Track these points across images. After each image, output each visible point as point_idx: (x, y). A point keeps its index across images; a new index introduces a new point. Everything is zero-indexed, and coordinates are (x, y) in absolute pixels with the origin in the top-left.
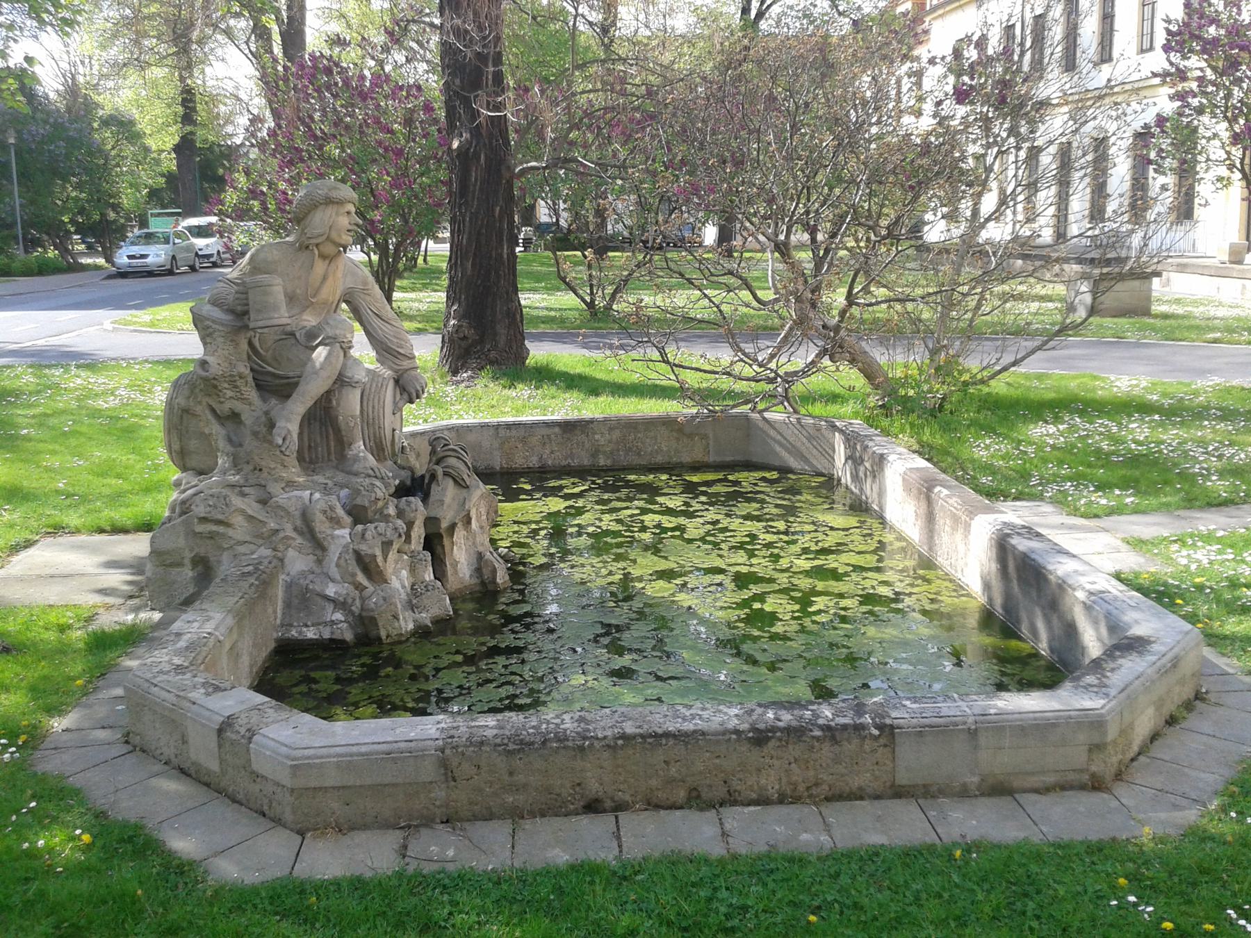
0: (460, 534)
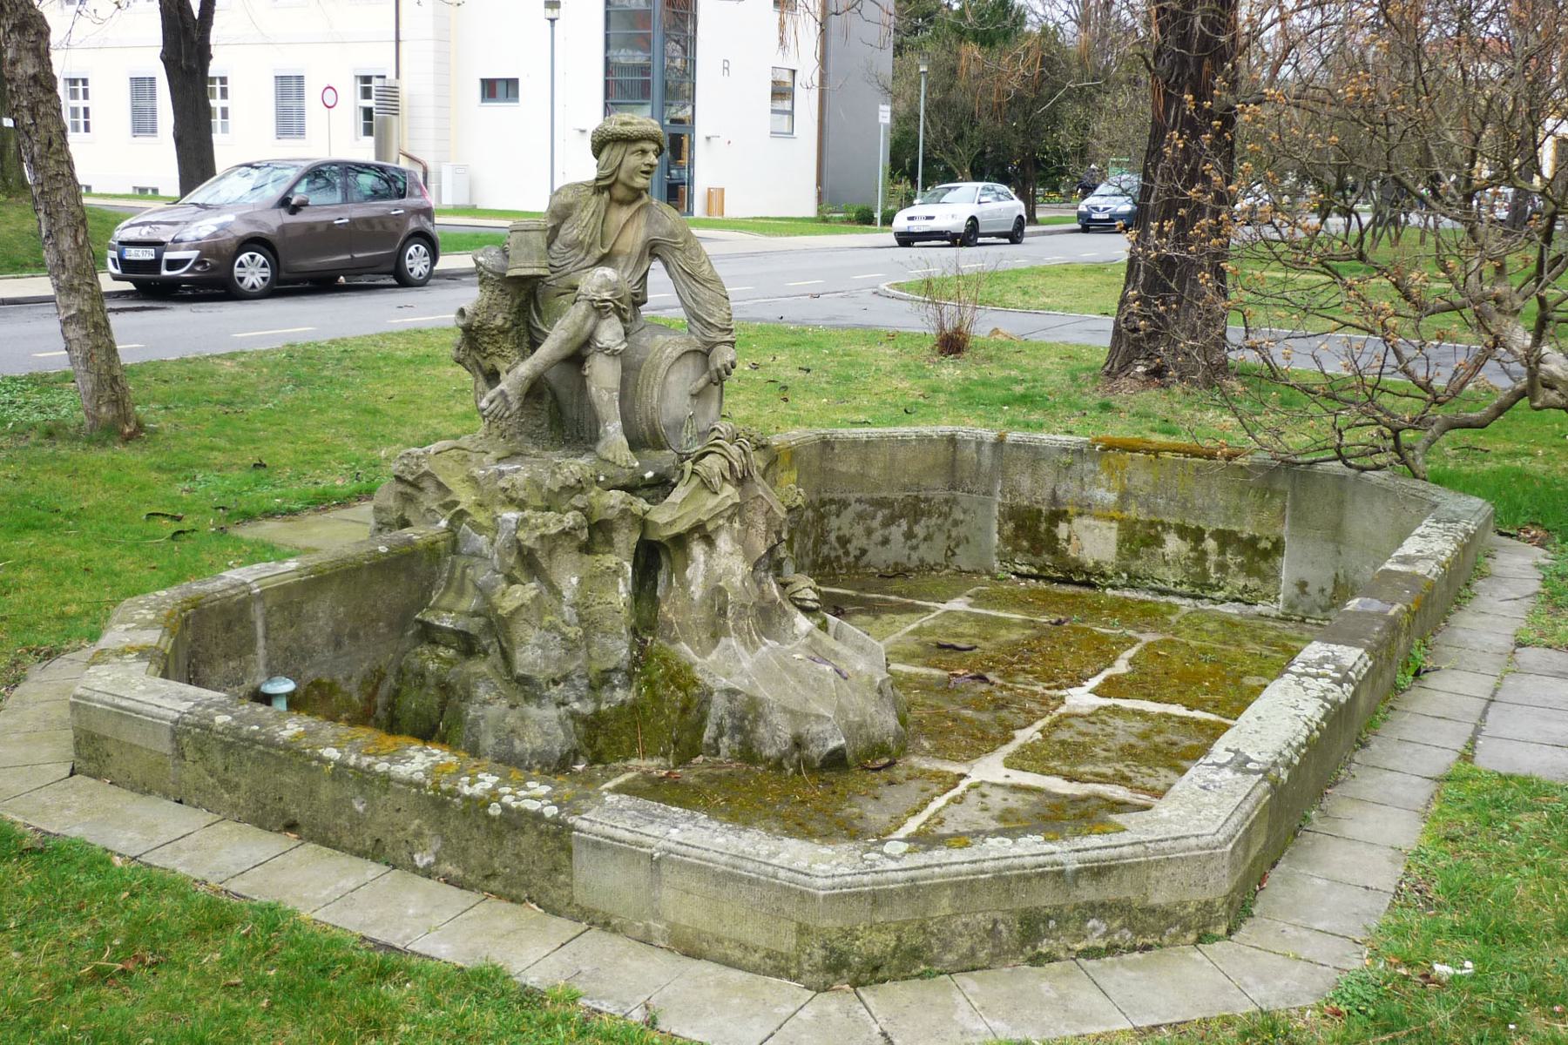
0: (698, 550)
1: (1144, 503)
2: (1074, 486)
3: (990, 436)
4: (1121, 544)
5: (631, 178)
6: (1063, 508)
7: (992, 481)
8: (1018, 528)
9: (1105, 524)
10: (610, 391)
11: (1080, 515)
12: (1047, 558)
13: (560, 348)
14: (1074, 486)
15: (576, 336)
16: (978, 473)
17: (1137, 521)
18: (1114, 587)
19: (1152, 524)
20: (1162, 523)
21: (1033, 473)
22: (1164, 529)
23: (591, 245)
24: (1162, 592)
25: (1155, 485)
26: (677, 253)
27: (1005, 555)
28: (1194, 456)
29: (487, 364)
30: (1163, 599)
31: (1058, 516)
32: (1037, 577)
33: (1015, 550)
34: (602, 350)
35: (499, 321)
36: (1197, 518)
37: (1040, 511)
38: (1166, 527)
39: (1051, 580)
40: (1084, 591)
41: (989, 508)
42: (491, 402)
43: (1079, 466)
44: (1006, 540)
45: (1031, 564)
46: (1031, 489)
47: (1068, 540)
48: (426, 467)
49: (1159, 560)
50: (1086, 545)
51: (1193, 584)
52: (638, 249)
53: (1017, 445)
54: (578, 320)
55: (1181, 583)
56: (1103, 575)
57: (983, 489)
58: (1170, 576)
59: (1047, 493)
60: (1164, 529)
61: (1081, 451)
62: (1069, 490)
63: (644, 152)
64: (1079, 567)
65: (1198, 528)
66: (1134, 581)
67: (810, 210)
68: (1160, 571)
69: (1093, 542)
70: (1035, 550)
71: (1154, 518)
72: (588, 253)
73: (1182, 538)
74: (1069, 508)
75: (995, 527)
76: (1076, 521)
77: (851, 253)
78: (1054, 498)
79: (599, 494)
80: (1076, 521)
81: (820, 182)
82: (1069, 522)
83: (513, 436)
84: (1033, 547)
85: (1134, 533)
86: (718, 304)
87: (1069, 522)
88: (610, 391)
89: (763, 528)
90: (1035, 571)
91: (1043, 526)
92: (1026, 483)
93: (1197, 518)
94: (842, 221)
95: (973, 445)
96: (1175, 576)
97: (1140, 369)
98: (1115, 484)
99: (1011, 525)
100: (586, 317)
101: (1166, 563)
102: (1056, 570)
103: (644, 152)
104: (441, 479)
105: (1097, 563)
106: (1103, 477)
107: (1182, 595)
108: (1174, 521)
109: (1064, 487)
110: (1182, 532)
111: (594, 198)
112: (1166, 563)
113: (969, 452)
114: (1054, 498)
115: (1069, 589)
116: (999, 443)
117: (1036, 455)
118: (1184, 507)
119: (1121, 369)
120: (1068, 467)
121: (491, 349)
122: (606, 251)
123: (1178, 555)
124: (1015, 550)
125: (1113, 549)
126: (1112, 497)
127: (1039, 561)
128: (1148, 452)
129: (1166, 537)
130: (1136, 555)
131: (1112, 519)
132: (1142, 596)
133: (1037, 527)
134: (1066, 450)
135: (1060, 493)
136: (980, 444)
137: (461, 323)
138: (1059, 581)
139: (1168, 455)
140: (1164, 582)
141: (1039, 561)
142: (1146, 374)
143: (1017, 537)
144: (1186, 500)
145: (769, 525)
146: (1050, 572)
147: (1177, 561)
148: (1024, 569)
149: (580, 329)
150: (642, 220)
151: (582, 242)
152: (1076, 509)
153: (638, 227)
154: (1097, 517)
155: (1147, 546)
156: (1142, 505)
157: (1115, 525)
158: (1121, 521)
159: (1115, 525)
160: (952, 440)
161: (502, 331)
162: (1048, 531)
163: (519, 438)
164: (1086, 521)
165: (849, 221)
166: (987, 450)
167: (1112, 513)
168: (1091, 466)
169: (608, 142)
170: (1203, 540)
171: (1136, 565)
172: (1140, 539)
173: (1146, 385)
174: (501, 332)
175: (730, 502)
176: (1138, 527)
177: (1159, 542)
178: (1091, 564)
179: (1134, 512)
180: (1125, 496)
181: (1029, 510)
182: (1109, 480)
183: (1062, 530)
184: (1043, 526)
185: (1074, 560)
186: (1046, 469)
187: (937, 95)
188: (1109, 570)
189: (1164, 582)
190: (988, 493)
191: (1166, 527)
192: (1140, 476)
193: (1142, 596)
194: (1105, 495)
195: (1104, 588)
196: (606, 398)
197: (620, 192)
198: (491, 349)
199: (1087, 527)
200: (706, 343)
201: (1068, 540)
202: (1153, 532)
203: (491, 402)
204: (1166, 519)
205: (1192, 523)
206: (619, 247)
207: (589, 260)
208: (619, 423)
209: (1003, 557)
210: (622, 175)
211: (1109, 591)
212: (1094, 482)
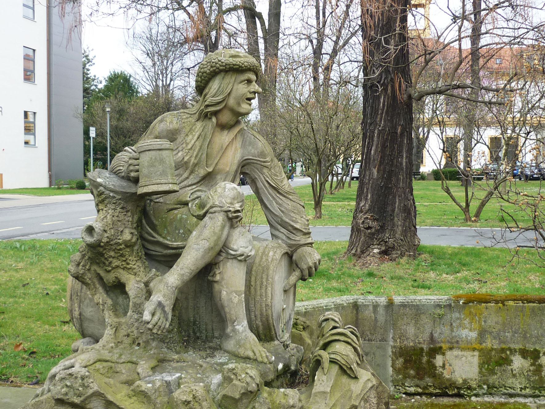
1: (497, 337)
2: (446, 330)
3: (383, 300)
4: (481, 366)
5: (239, 104)
6: (438, 345)
7: (386, 331)
8: (406, 361)
9: (468, 354)
10: (238, 293)
11: (451, 349)
12: (429, 381)
13: (203, 257)
14: (446, 330)
15: (216, 245)
16: (375, 327)
17: (492, 349)
18: (476, 395)
19: (503, 350)
20: (510, 349)
21: (416, 322)
22: (511, 353)
23: (195, 165)
24: (511, 396)
25: (504, 324)
26: (265, 171)
27: (398, 381)
28: (530, 302)
29: (110, 278)
30: (512, 400)
31: (435, 351)
32: (420, 394)
33: (405, 377)
34: (235, 257)
35: (127, 236)
36: (534, 344)
37: (422, 349)
38: (513, 351)
39: (431, 395)
40: (457, 400)
41: (385, 350)
42: (153, 315)
43: (449, 316)
44: (397, 371)
45: (417, 386)
46: (415, 335)
47: (444, 367)
48: (95, 387)
49: (509, 374)
50: (456, 368)
51: (534, 388)
52: (234, 167)
53: (403, 305)
54: (217, 230)
55: (525, 388)
56: (469, 388)
57: (379, 337)
58: (517, 384)
59: (426, 336)
60: (511, 353)
61: (450, 306)
62: (442, 333)
63: (249, 81)
64: (452, 384)
65: (535, 350)
66: (492, 390)
67: (44, 182)
68: (510, 381)
69: (461, 366)
70: (420, 375)
71: (504, 346)
72: (192, 172)
73: (524, 357)
74: (443, 345)
75: (390, 363)
76: (449, 353)
77: (86, 203)
78: (432, 339)
79: (270, 394)
80: (449, 353)
81: (50, 170)
82: (444, 354)
83: (147, 342)
84: (418, 374)
85: (491, 358)
86: (299, 213)
87: (444, 354)
88: (238, 293)
89: (374, 401)
90: (420, 390)
91: (425, 359)
92: (411, 330)
93: (534, 344)
94: (67, 188)
95: (371, 308)
96: (520, 383)
97: (376, 251)
98: (475, 325)
99: (401, 360)
100: (223, 227)
101: (514, 376)
102: (435, 388)
103: (249, 81)
104: (110, 398)
105: (465, 381)
106: (466, 322)
107: (525, 396)
108: (517, 347)
109: (439, 331)
110: (524, 353)
111: (199, 125)
112: (514, 376)
113: (368, 313)
114: (432, 339)
115: (445, 401)
116: (390, 304)
117: (417, 311)
118: (525, 337)
119: (363, 252)
120: (441, 317)
121: (116, 263)
122: (210, 170)
123: (522, 369)
124: (405, 377)
125: (476, 369)
126: (473, 335)
127: (422, 383)
128: (497, 302)
129: (513, 358)
130: (492, 372)
131: (474, 349)
132: (497, 399)
133: (420, 360)
134: (439, 306)
135: (436, 335)
136: (376, 306)
137: (89, 240)
138: (436, 395)
139: (511, 303)
140: (513, 388)
141: (422, 383)
142: (380, 253)
143: (406, 368)
144: (526, 332)
145: (379, 398)
146: (431, 390)
147: (521, 373)
148: (412, 390)
149: (219, 238)
150: (238, 144)
151: (186, 163)
152: (448, 345)
153: (236, 150)
154: (463, 349)
155: (500, 365)
156: (495, 338)
157: (476, 353)
158: (480, 350)
159: (476, 353)
160: (356, 306)
161: (129, 245)
162: (429, 362)
163: (154, 344)
164: (455, 352)
165: (72, 188)
166: (381, 311)
167: (474, 346)
168: (457, 315)
169: (221, 71)
170: (539, 357)
171: (492, 379)
172: (494, 361)
173: (382, 261)
174: (127, 246)
175: (370, 385)
176: (493, 353)
177: (508, 362)
178: (461, 381)
179: (490, 343)
180: (482, 334)
181: (414, 349)
182: (471, 323)
183: (439, 360)
184: (425, 359)
185: (448, 380)
186: (425, 320)
187: (115, 123)
188: (474, 384)
189: (513, 388)
190: (384, 340)
191: (513, 351)
192: (492, 318)
193: (497, 399)
194: (468, 334)
195: (470, 397)
196: (236, 300)
197: (226, 117)
198: (116, 263)
199: (456, 357)
200: (290, 246)
201: (444, 367)
202: (503, 355)
203: (153, 315)
204: (512, 346)
205: (531, 347)
206: (220, 166)
207: (193, 179)
208: (245, 323)
209: (396, 383)
210: (231, 102)
211: (473, 399)
212: (461, 326)
